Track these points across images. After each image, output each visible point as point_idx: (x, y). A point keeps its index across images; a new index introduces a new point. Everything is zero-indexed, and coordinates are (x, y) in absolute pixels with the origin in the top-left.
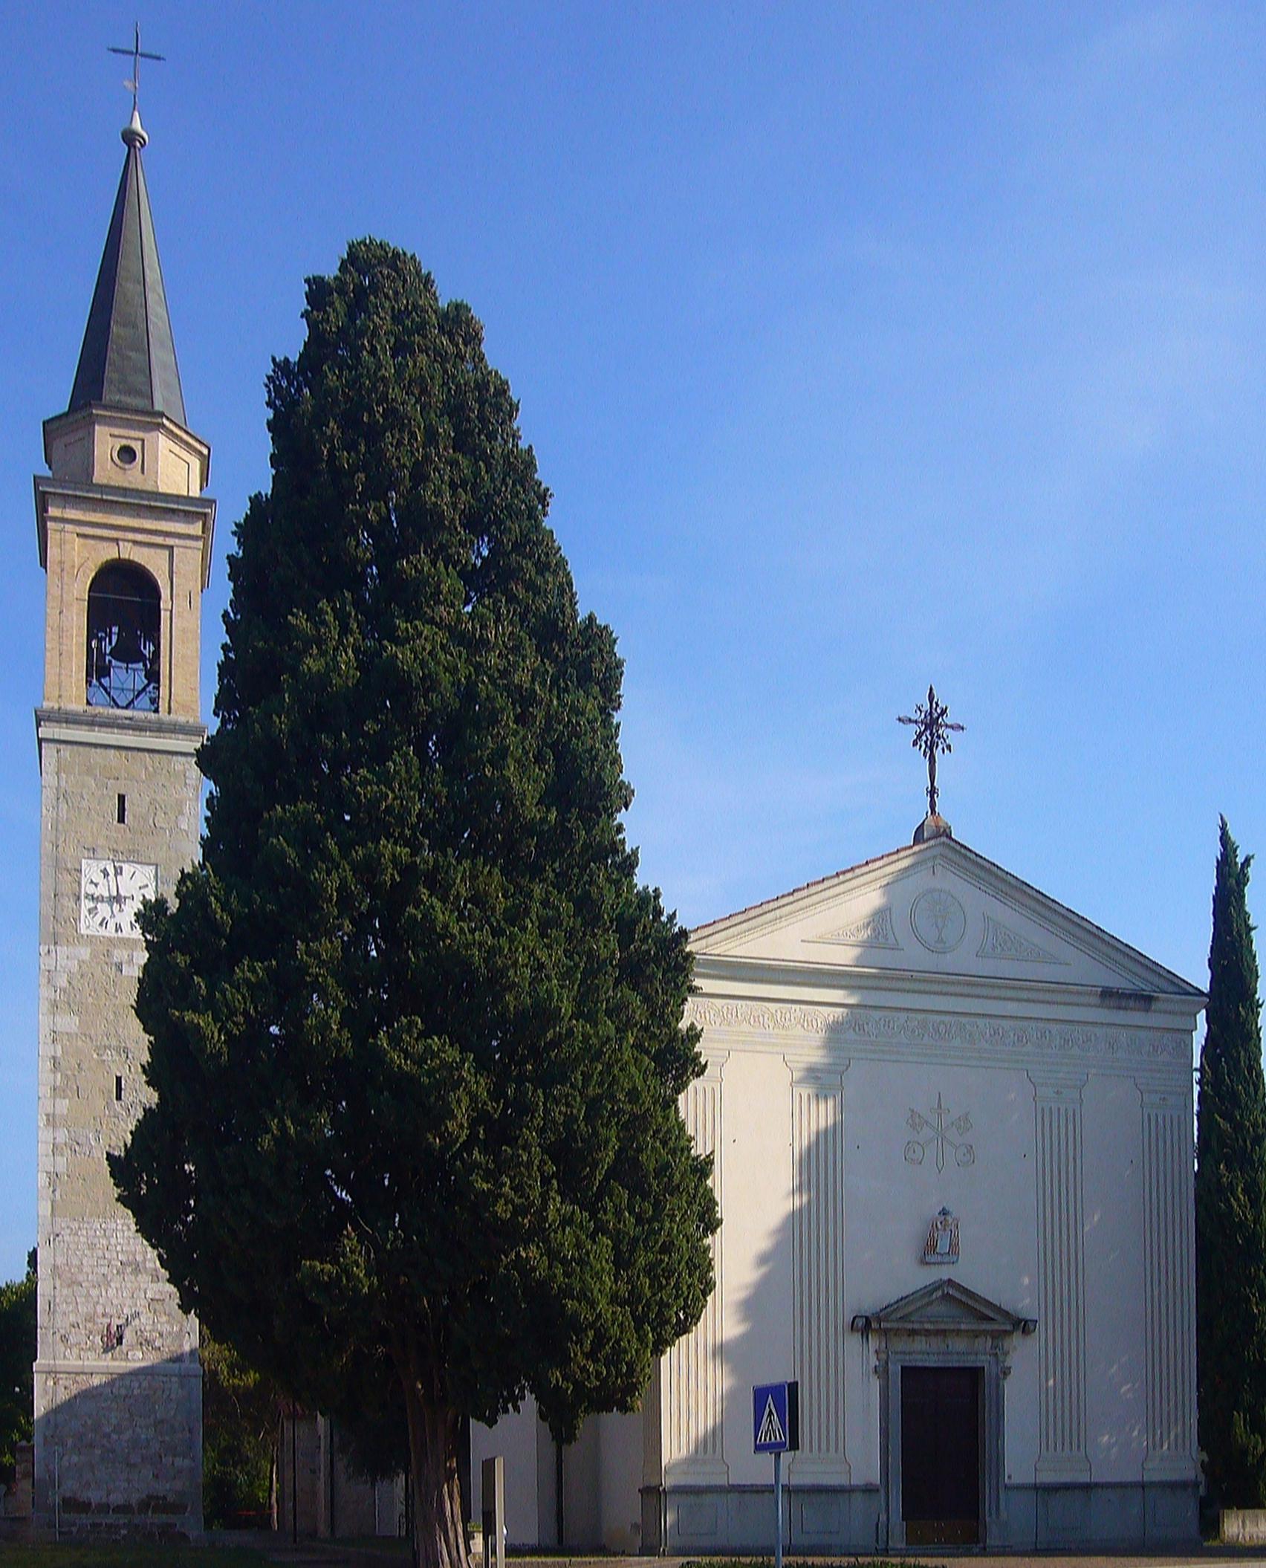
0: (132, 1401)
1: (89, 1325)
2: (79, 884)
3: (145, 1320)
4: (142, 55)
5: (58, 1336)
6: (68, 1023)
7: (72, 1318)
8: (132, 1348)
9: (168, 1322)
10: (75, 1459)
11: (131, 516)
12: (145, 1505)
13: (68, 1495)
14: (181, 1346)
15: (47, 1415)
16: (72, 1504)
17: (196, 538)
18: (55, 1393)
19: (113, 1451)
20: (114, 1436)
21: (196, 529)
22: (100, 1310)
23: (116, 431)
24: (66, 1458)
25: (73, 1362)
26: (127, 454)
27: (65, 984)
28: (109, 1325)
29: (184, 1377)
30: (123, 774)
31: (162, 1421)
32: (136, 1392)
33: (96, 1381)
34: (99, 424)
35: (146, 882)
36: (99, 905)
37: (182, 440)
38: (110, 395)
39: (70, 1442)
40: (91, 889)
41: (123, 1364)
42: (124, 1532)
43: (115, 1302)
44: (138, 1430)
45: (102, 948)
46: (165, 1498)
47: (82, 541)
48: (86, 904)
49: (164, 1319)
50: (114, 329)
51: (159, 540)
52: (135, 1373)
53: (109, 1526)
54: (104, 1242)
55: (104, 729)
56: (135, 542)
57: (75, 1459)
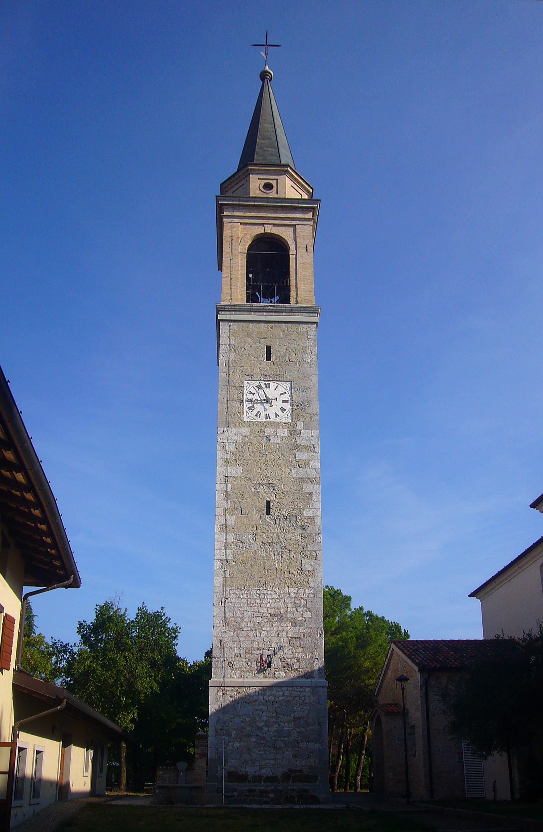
0: (277, 705)
1: (248, 655)
2: (243, 394)
3: (287, 651)
4: (269, 46)
5: (226, 662)
6: (235, 471)
7: (237, 651)
8: (277, 669)
9: (303, 652)
10: (237, 744)
11: (270, 213)
12: (287, 777)
13: (232, 769)
14: (312, 667)
15: (218, 712)
16: (233, 776)
17: (309, 220)
18: (223, 700)
19: (264, 739)
20: (265, 729)
21: (310, 215)
22: (255, 645)
23: (262, 177)
24: (231, 743)
25: (236, 680)
26: (268, 187)
27: (233, 449)
28: (262, 655)
29: (313, 688)
30: (270, 335)
31: (299, 718)
32: (281, 698)
33: (252, 690)
34: (252, 174)
35: (285, 391)
36: (255, 405)
37: (299, 183)
38: (257, 158)
39: (234, 733)
40: (250, 397)
41: (272, 680)
42: (271, 795)
43: (266, 640)
44: (283, 724)
45: (258, 428)
46: (301, 771)
47: (243, 226)
48: (247, 405)
49: (300, 650)
50: (259, 141)
51: (288, 222)
52: (278, 685)
53: (261, 791)
54: (258, 601)
55: (257, 313)
56: (274, 225)
57: (237, 744)
